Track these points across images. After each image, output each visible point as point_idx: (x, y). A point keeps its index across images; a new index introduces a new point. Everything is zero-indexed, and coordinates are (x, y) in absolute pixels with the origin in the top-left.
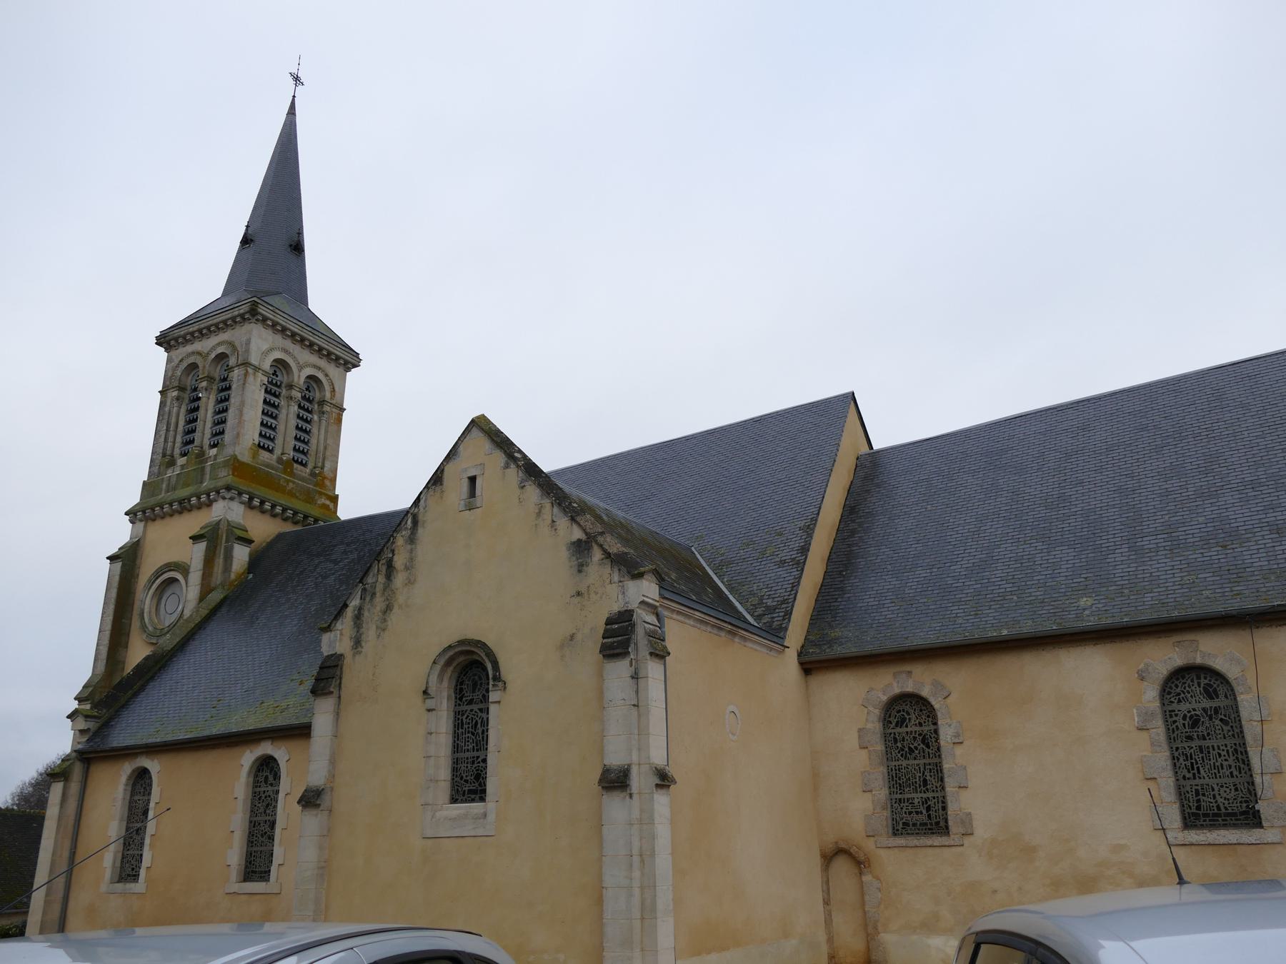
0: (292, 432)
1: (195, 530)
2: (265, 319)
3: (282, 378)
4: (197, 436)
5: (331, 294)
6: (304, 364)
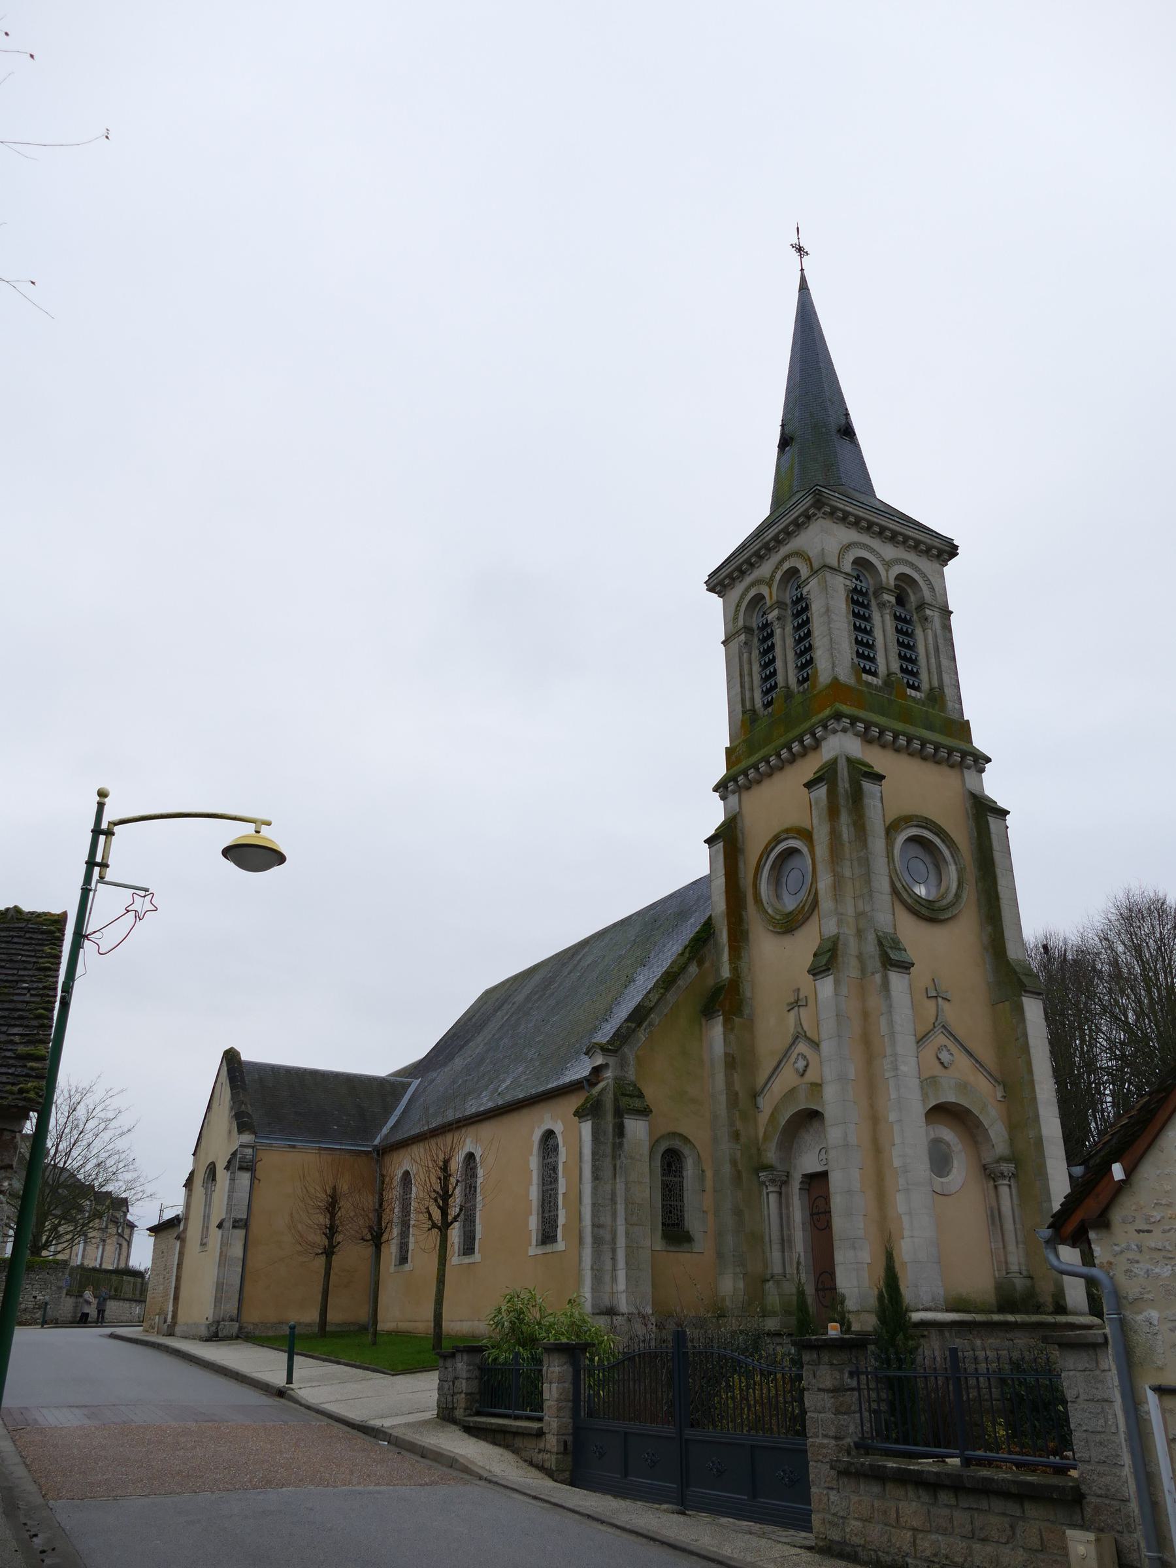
0: (894, 649)
1: (809, 776)
2: (834, 510)
3: (867, 584)
4: (780, 677)
5: (901, 471)
6: (890, 562)
